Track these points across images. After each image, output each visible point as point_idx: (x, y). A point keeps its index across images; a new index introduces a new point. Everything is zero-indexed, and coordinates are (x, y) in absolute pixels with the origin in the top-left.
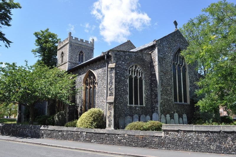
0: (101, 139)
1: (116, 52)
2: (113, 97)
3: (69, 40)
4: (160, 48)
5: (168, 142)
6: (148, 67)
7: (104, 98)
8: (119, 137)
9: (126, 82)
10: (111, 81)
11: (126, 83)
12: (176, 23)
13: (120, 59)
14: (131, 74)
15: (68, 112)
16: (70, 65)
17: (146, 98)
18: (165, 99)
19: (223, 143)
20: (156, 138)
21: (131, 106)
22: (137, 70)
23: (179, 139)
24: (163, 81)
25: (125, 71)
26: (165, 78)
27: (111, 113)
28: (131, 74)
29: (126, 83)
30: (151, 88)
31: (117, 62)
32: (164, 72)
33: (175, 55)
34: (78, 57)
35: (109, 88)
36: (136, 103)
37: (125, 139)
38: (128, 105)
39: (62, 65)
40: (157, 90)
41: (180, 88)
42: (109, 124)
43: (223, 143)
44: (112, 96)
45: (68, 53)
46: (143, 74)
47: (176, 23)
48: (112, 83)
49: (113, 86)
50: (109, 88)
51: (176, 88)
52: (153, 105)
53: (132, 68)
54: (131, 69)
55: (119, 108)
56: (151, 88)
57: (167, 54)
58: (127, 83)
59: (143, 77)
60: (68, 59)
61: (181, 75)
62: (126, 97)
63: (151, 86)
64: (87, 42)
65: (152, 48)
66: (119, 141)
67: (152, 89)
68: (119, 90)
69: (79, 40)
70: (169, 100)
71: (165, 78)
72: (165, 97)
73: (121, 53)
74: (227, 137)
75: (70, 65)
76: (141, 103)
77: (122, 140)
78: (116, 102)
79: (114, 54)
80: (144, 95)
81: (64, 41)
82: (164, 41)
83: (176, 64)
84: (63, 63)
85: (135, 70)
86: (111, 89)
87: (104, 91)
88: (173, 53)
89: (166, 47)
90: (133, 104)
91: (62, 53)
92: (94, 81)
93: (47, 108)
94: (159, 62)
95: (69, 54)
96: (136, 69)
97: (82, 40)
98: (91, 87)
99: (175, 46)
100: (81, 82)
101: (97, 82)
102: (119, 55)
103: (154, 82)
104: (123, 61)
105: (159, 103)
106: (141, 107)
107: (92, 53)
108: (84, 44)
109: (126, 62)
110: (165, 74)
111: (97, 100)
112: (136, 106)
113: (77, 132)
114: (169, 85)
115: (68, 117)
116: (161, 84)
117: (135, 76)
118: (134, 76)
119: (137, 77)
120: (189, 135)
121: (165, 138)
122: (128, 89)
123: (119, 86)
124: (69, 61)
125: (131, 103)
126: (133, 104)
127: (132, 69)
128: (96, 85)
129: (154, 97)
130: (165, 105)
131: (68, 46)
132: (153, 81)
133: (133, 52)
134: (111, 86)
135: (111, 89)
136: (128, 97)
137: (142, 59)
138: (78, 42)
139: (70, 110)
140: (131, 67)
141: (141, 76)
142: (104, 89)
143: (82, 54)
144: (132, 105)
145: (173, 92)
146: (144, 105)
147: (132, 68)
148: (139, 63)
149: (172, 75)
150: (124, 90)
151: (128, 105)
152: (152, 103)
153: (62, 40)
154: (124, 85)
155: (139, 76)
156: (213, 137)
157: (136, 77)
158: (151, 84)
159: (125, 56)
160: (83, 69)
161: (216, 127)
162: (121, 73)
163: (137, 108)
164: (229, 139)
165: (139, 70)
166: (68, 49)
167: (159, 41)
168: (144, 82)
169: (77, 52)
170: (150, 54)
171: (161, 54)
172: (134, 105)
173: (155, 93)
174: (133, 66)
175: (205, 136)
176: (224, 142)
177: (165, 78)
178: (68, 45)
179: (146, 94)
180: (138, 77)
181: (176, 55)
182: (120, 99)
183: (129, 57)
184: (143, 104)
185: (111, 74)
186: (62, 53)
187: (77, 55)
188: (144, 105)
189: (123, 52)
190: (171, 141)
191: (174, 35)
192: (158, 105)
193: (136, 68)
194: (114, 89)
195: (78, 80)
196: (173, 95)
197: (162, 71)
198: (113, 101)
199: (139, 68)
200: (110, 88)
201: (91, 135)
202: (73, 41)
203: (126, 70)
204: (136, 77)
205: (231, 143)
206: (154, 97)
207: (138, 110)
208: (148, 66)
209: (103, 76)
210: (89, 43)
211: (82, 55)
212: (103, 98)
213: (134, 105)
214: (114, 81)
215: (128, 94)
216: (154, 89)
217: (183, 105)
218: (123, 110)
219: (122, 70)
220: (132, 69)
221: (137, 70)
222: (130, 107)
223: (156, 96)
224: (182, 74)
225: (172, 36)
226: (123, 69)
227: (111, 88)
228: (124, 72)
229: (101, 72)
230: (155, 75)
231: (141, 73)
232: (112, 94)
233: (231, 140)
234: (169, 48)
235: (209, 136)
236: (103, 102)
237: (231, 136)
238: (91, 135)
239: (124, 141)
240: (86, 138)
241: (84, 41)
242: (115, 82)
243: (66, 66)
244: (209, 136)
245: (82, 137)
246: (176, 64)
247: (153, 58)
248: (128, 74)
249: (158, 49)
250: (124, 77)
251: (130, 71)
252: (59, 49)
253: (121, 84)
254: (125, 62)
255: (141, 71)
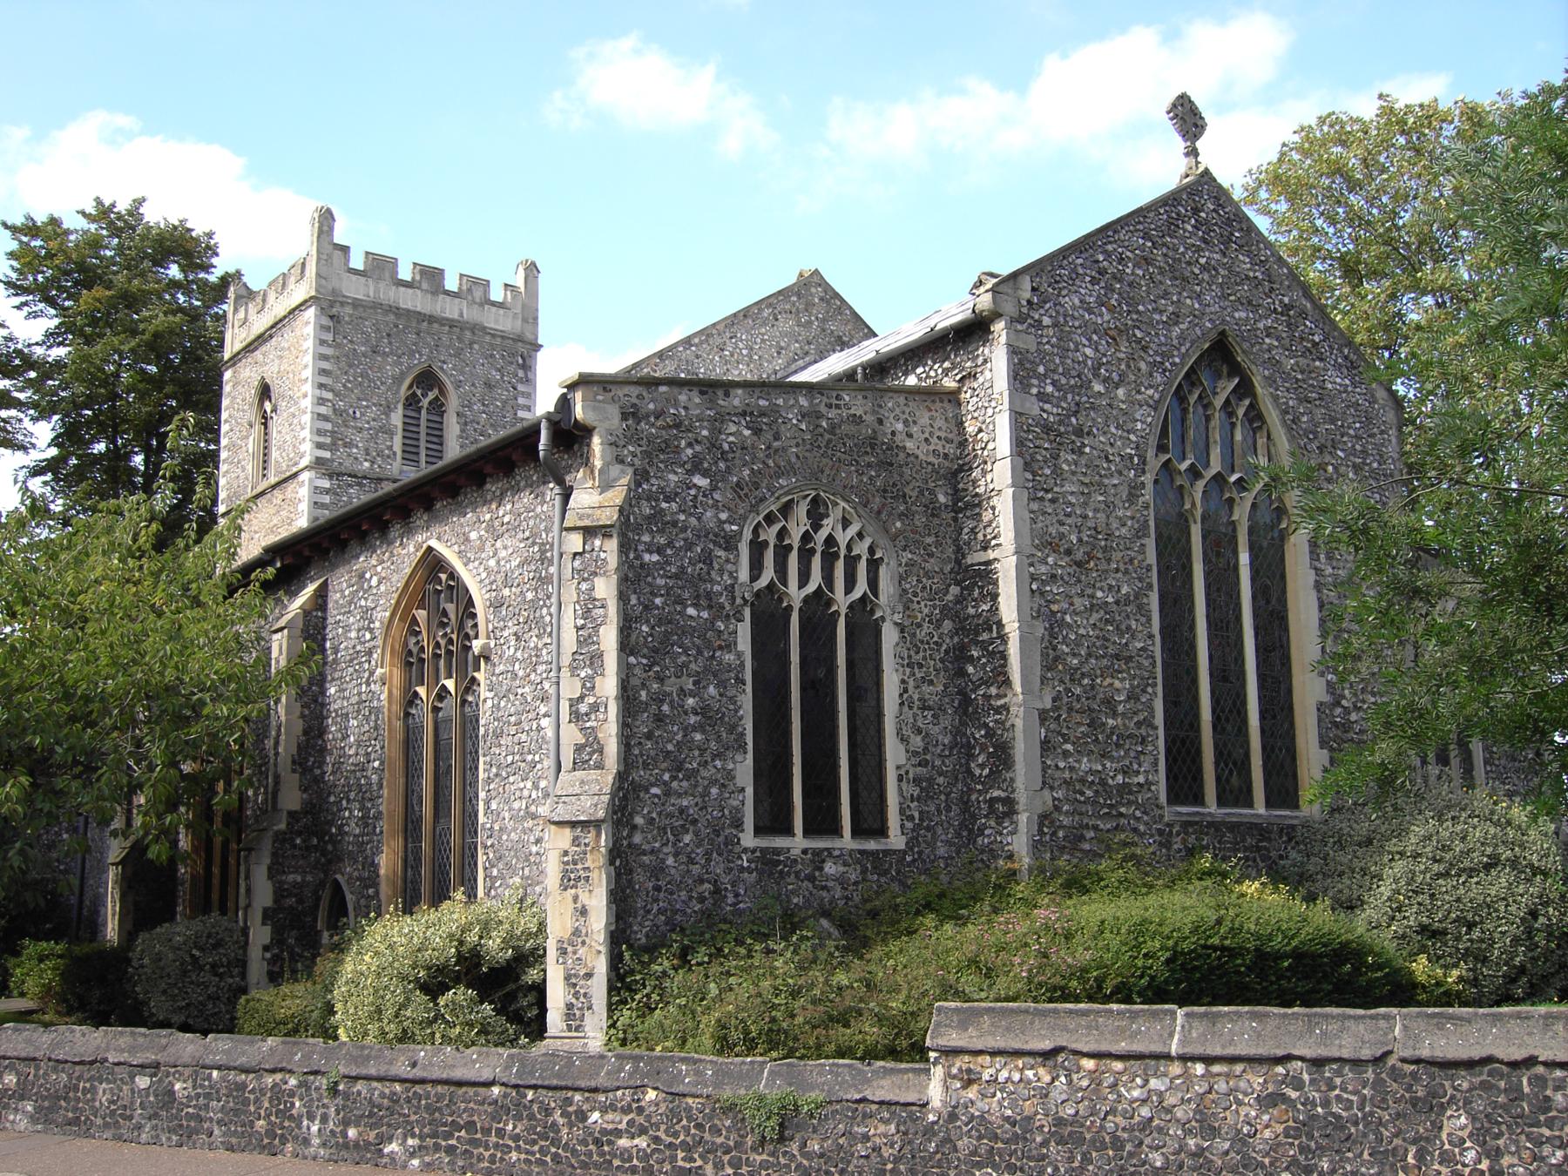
0: (456, 1126)
1: (634, 391)
2: (606, 779)
3: (318, 275)
4: (1029, 343)
5: (974, 1153)
6: (933, 510)
7: (543, 784)
8: (595, 1116)
9: (730, 646)
10: (587, 638)
11: (729, 657)
12: (1187, 117)
13: (668, 447)
14: (768, 575)
15: (265, 910)
16: (327, 499)
17: (917, 781)
18: (1083, 781)
19: (1410, 1160)
20: (886, 1122)
21: (777, 851)
22: (830, 541)
23: (1059, 1122)
24: (1062, 624)
25: (721, 553)
26: (1079, 603)
27: (584, 912)
28: (768, 575)
29: (729, 657)
30: (962, 693)
31: (641, 476)
32: (1068, 552)
33: (1180, 396)
34: (397, 418)
35: (574, 703)
36: (822, 821)
37: (643, 1131)
38: (748, 839)
39: (262, 494)
40: (1006, 708)
41: (1225, 679)
42: (570, 1006)
43: (1410, 1160)
44: (600, 766)
45: (308, 388)
46: (883, 570)
47: (1187, 117)
48: (596, 659)
49: (609, 685)
50: (574, 703)
51: (1195, 681)
52: (981, 832)
53: (777, 527)
54: (771, 535)
55: (658, 871)
56: (962, 693)
57: (1098, 387)
58: (739, 655)
59: (883, 599)
60: (307, 447)
61: (1236, 568)
62: (730, 775)
63: (962, 673)
64: (478, 294)
65: (972, 331)
66: (597, 1142)
67: (966, 701)
68: (659, 719)
69: (405, 273)
70: (1124, 788)
71: (1078, 602)
72: (1085, 764)
73: (683, 398)
74: (1433, 1106)
75: (327, 499)
76: (870, 823)
77: (618, 1133)
78: (639, 820)
79: (614, 412)
80: (894, 754)
81: (282, 282)
82: (1075, 275)
83: (1195, 473)
84: (273, 480)
85: (806, 538)
86: (583, 708)
87: (539, 729)
88: (1159, 378)
89: (1089, 329)
90: (788, 831)
91: (265, 392)
92: (467, 637)
93: (112, 874)
94: (1027, 466)
95: (321, 401)
96: (822, 534)
97: (431, 276)
98: (443, 693)
99: (1176, 318)
100: (370, 653)
101: (485, 647)
102: (659, 415)
103: (985, 636)
104: (696, 467)
105: (1023, 818)
106: (862, 852)
107: (521, 388)
108: (451, 309)
109: (728, 470)
110: (1079, 564)
111: (487, 803)
112: (817, 853)
113: (273, 1071)
114: (1117, 657)
115: (266, 948)
116: (1044, 655)
117: (811, 588)
118: (795, 594)
119: (830, 602)
120: (1136, 1093)
121: (953, 1117)
122: (746, 701)
123: (661, 679)
124: (318, 463)
125: (774, 820)
126: (788, 831)
127: (783, 533)
128: (480, 676)
129: (982, 766)
130: (1082, 838)
131: (310, 330)
132: (977, 634)
133: (809, 387)
134: (589, 687)
135: (583, 708)
136: (744, 769)
137: (872, 442)
138: (391, 295)
139: (279, 894)
140: (770, 520)
141: (861, 588)
142: (543, 709)
143: (431, 395)
144: (780, 842)
145: (1159, 719)
146: (896, 839)
147: (777, 527)
148: (851, 477)
149: (1149, 568)
150: (703, 711)
151: (748, 839)
152: (974, 817)
153: (255, 281)
154: (706, 669)
155: (849, 588)
156: (1326, 1103)
157: (819, 600)
158: (959, 656)
159: (720, 419)
160: (474, 511)
161: (1350, 1024)
162: (682, 568)
163: (830, 868)
164: (1457, 1122)
165: (842, 538)
166: (309, 359)
167: (1026, 283)
168: (890, 637)
169: (395, 372)
170: (953, 397)
171: (1042, 396)
172: (797, 843)
173: (990, 733)
174: (786, 509)
175: (1269, 1101)
176: (1412, 1150)
177: (1079, 603)
178: (308, 324)
179: (917, 742)
180: (842, 601)
181: (1193, 398)
182: (668, 793)
183: (757, 432)
184: (882, 832)
185: (584, 586)
186: (265, 392)
187: (388, 410)
188: (896, 839)
189: (702, 393)
190: (996, 1138)
191: (1172, 226)
192: (1013, 833)
193: (817, 527)
194: (613, 709)
195: (347, 629)
196: (1161, 743)
197: (1050, 544)
198: (601, 814)
199: (846, 523)
200: (581, 698)
201: (382, 1095)
202: (356, 289)
203: (730, 543)
204: (819, 600)
205: (1470, 1156)
206: (982, 766)
207: (842, 881)
208: (934, 501)
209: (530, 596)
210: (497, 294)
211: (438, 407)
212: (529, 784)
213: (797, 843)
214: (609, 638)
215: (742, 747)
216: (987, 697)
217: (1260, 830)
218: (702, 881)
219: (689, 546)
220: (783, 533)
221: (830, 541)
222: (768, 862)
223: (1002, 755)
224: (1244, 558)
225: (1146, 236)
226: (703, 533)
227: (591, 700)
228: (707, 559)
229: (514, 564)
230: (985, 576)
231: (862, 569)
232: (601, 751)
233: (1471, 1135)
234: (1114, 336)
235: (1294, 1095)
236: (534, 817)
237: (1467, 1102)
238: (382, 1095)
239: (636, 1141)
240: (346, 1123)
241: (451, 284)
242: (625, 647)
243: (295, 502)
244: (1294, 1095)
245: (311, 1118)
246: (1195, 473)
247: (971, 428)
248: (744, 575)
249: (1013, 350)
250: (707, 600)
251: (757, 548)
252: (236, 359)
253: (685, 665)
254: (716, 479)
255: (861, 549)
